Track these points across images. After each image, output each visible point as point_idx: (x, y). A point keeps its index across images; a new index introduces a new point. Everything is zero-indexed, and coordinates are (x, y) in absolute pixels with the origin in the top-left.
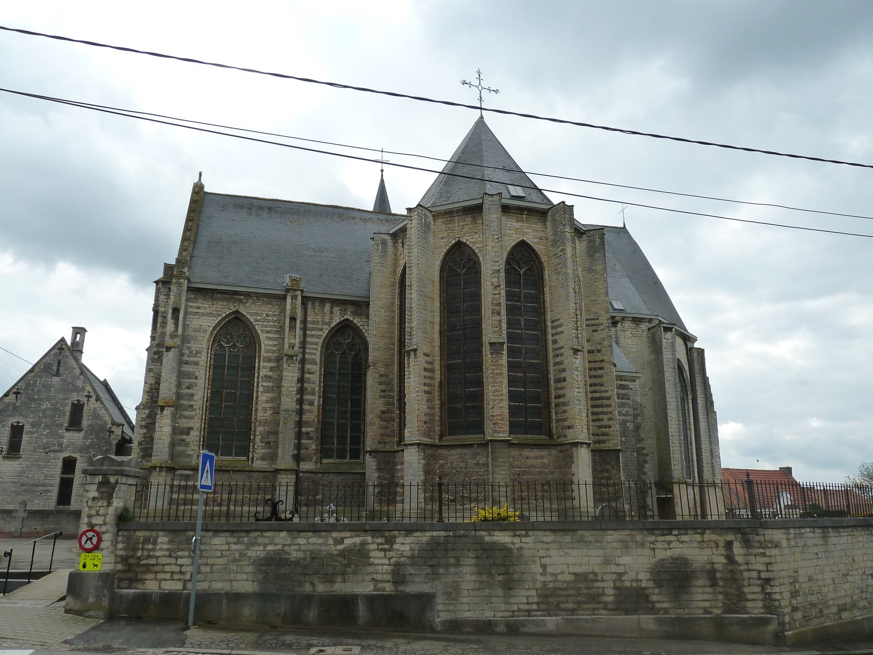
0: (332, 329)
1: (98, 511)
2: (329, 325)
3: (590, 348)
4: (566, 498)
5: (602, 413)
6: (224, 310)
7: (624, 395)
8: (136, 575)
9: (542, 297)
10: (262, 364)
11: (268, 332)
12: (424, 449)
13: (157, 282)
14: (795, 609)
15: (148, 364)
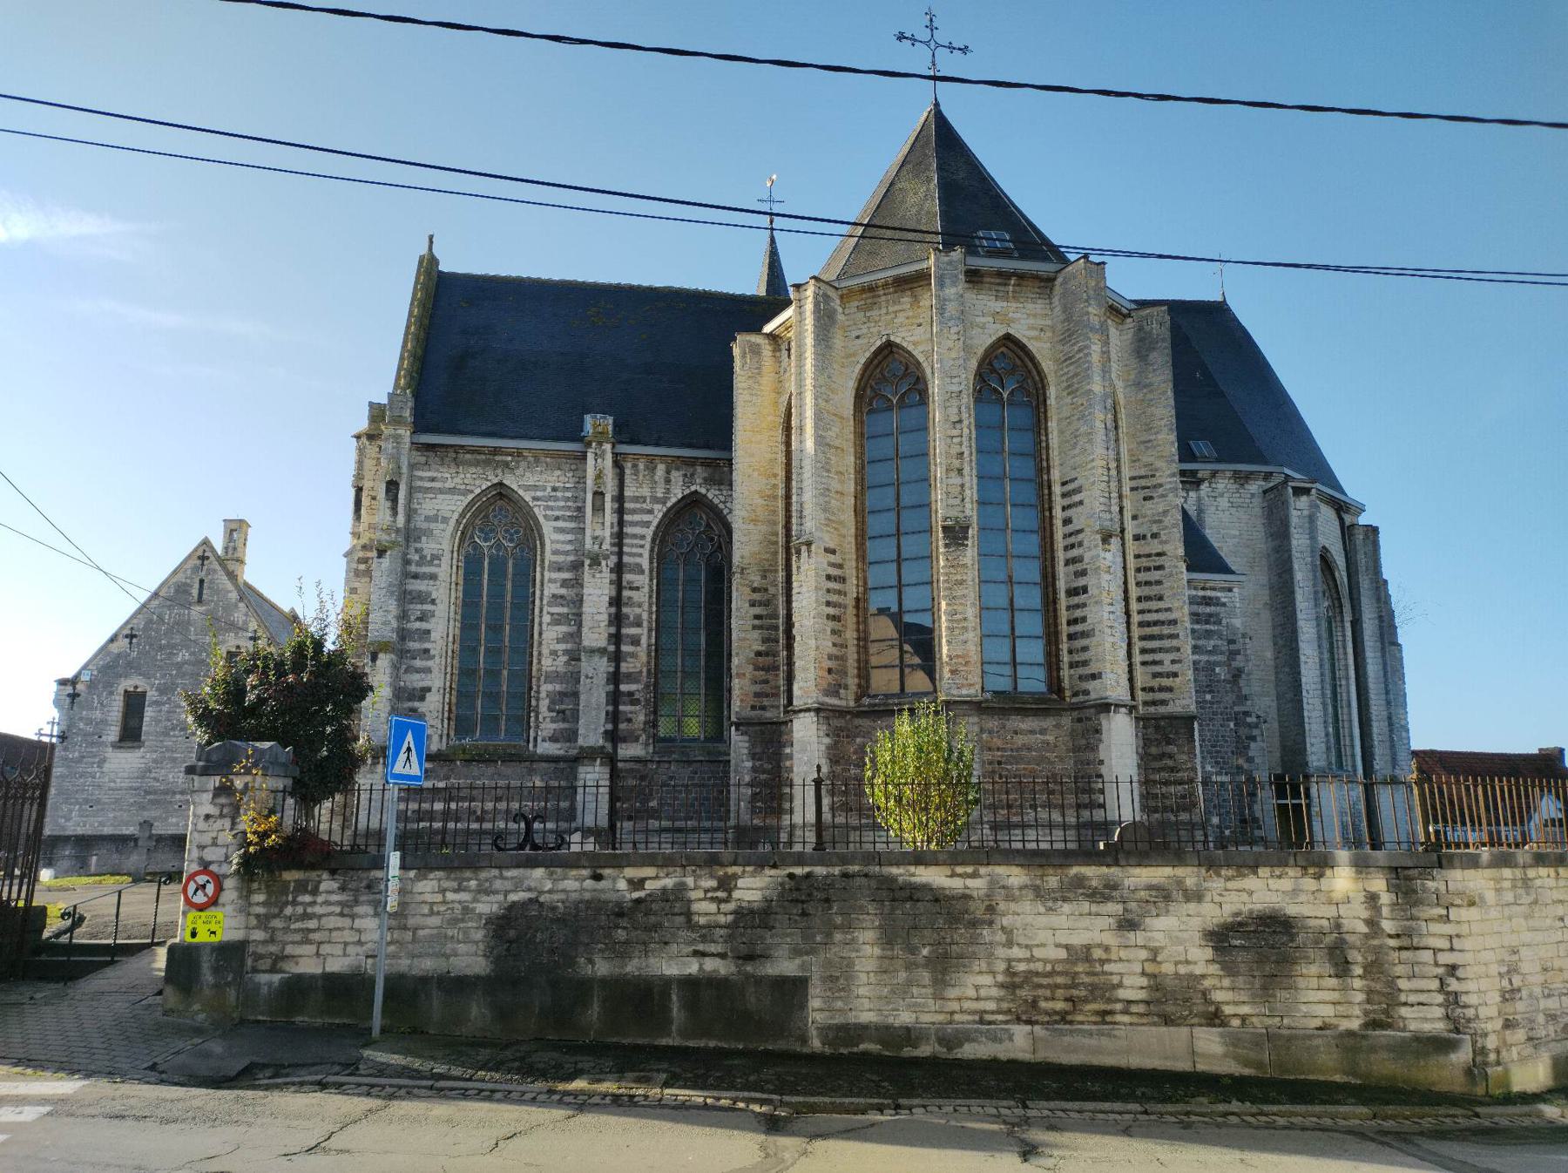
0: (669, 510)
1: (215, 839)
2: (664, 503)
3: (1140, 531)
4: (1092, 805)
5: (1161, 650)
6: (477, 482)
7: (1210, 615)
8: (284, 949)
9: (1044, 438)
10: (547, 574)
11: (557, 519)
12: (828, 718)
13: (358, 437)
14: (1508, 1024)
15: (347, 581)
